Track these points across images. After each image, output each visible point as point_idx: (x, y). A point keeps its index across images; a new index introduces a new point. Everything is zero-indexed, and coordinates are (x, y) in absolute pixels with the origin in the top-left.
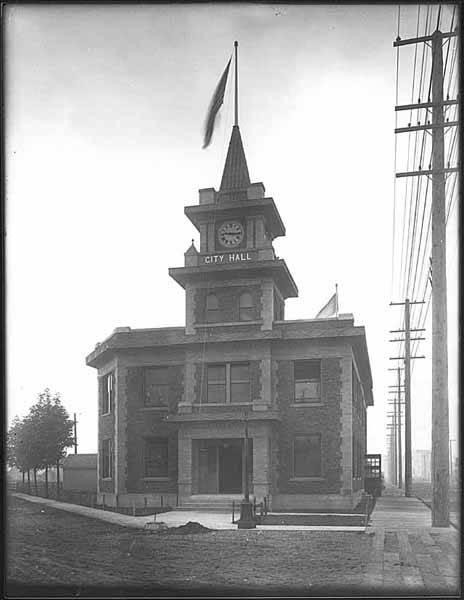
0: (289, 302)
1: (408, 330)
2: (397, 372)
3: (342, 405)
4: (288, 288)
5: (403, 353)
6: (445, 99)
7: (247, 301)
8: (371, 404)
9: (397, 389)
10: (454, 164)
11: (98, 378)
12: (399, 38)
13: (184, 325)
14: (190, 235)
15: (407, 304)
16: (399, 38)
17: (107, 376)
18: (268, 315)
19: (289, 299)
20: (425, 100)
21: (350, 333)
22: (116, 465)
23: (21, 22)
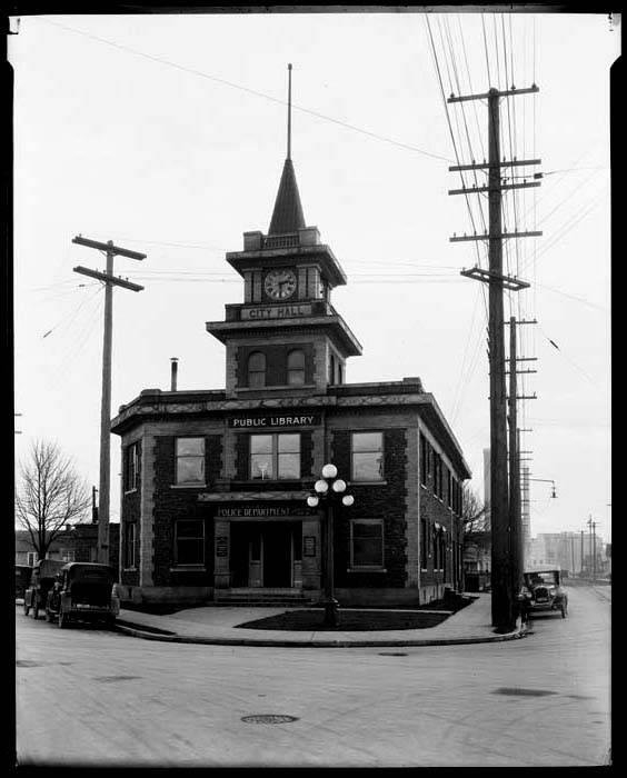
0: (350, 361)
1: (494, 165)
2: (483, 107)
3: (153, 522)
4: (348, 347)
5: (483, 226)
6: (502, 161)
7: (296, 359)
8: (406, 495)
9: (519, 366)
10: (505, 326)
11: (122, 447)
12: (452, 95)
13: (224, 388)
14: (235, 289)
15: (493, 97)
16: (452, 95)
17: (133, 445)
18: (324, 378)
19: (351, 358)
20: (480, 233)
21: (414, 399)
22: (141, 552)
23: (31, 37)
